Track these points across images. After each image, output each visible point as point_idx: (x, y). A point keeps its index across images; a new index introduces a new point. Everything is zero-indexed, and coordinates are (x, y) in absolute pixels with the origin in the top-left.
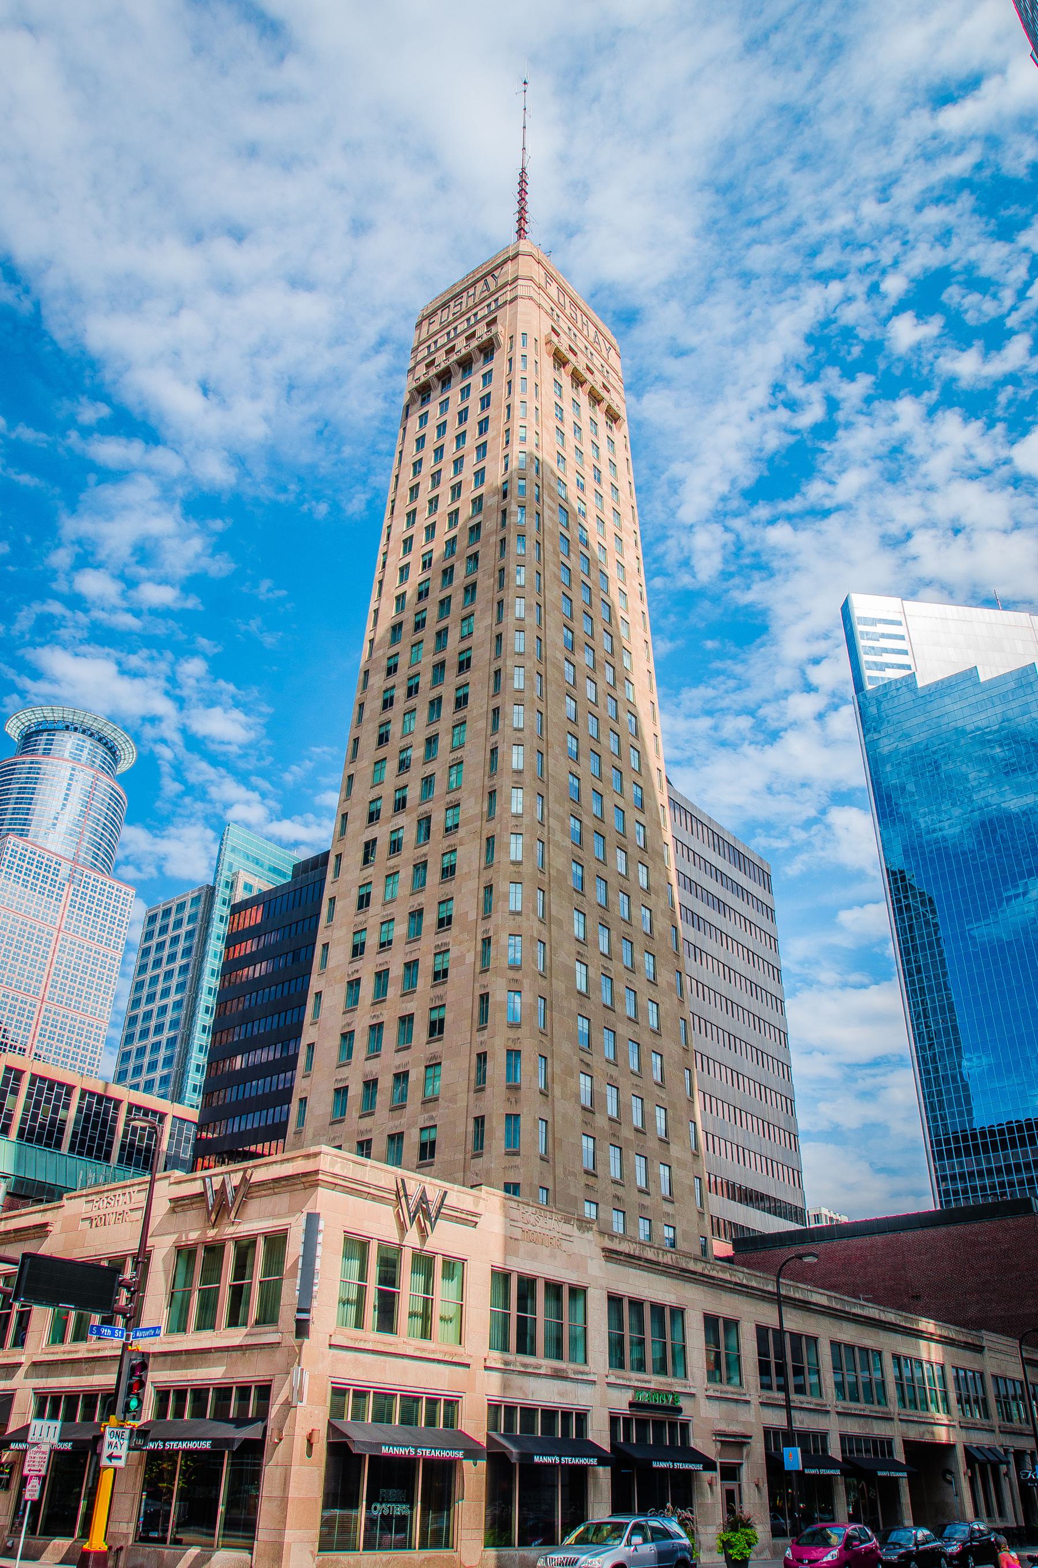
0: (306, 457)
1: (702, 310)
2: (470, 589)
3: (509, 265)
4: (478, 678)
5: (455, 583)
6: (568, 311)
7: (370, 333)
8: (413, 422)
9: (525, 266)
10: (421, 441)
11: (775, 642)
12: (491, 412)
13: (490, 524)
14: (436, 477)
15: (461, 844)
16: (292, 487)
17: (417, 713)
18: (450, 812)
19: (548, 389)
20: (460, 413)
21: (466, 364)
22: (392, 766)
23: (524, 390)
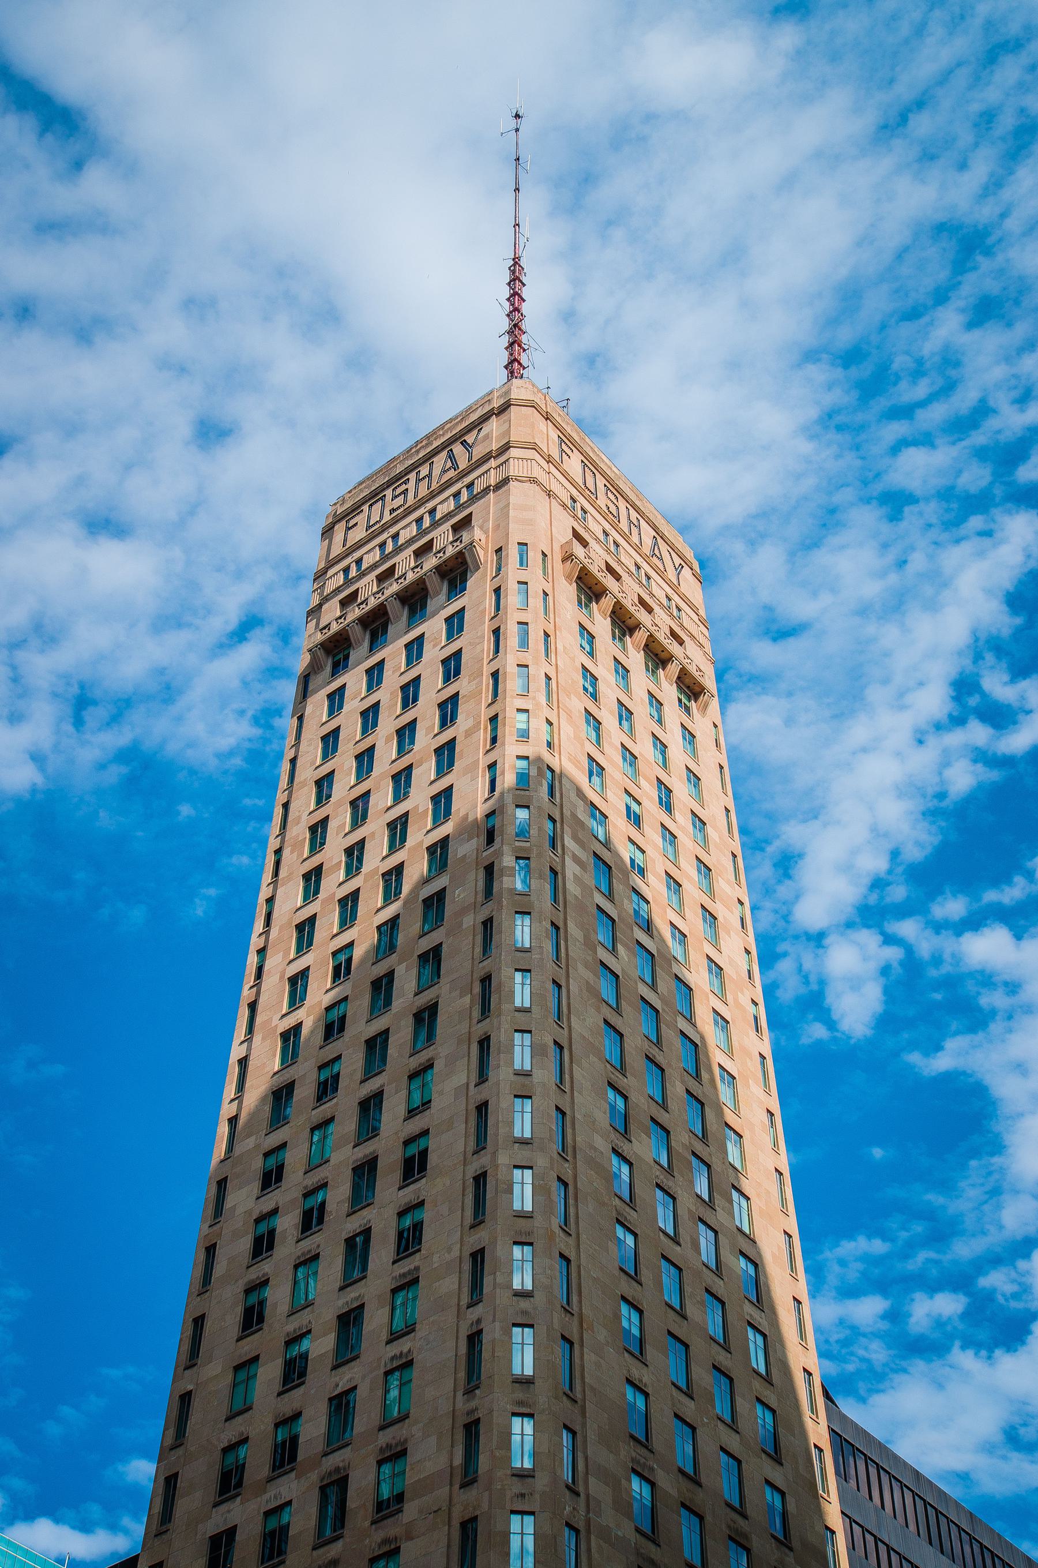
0: (106, 821)
1: (822, 557)
2: (426, 1018)
3: (494, 426)
4: (443, 1189)
5: (397, 1004)
6: (602, 502)
7: (231, 604)
8: (317, 705)
9: (522, 425)
10: (331, 741)
11: (998, 1147)
12: (462, 685)
13: (463, 893)
14: (360, 807)
15: (410, 1537)
16: (80, 876)
17: (322, 1264)
18: (386, 1469)
19: (568, 640)
20: (404, 688)
21: (415, 600)
22: (270, 1372)
23: (524, 643)
